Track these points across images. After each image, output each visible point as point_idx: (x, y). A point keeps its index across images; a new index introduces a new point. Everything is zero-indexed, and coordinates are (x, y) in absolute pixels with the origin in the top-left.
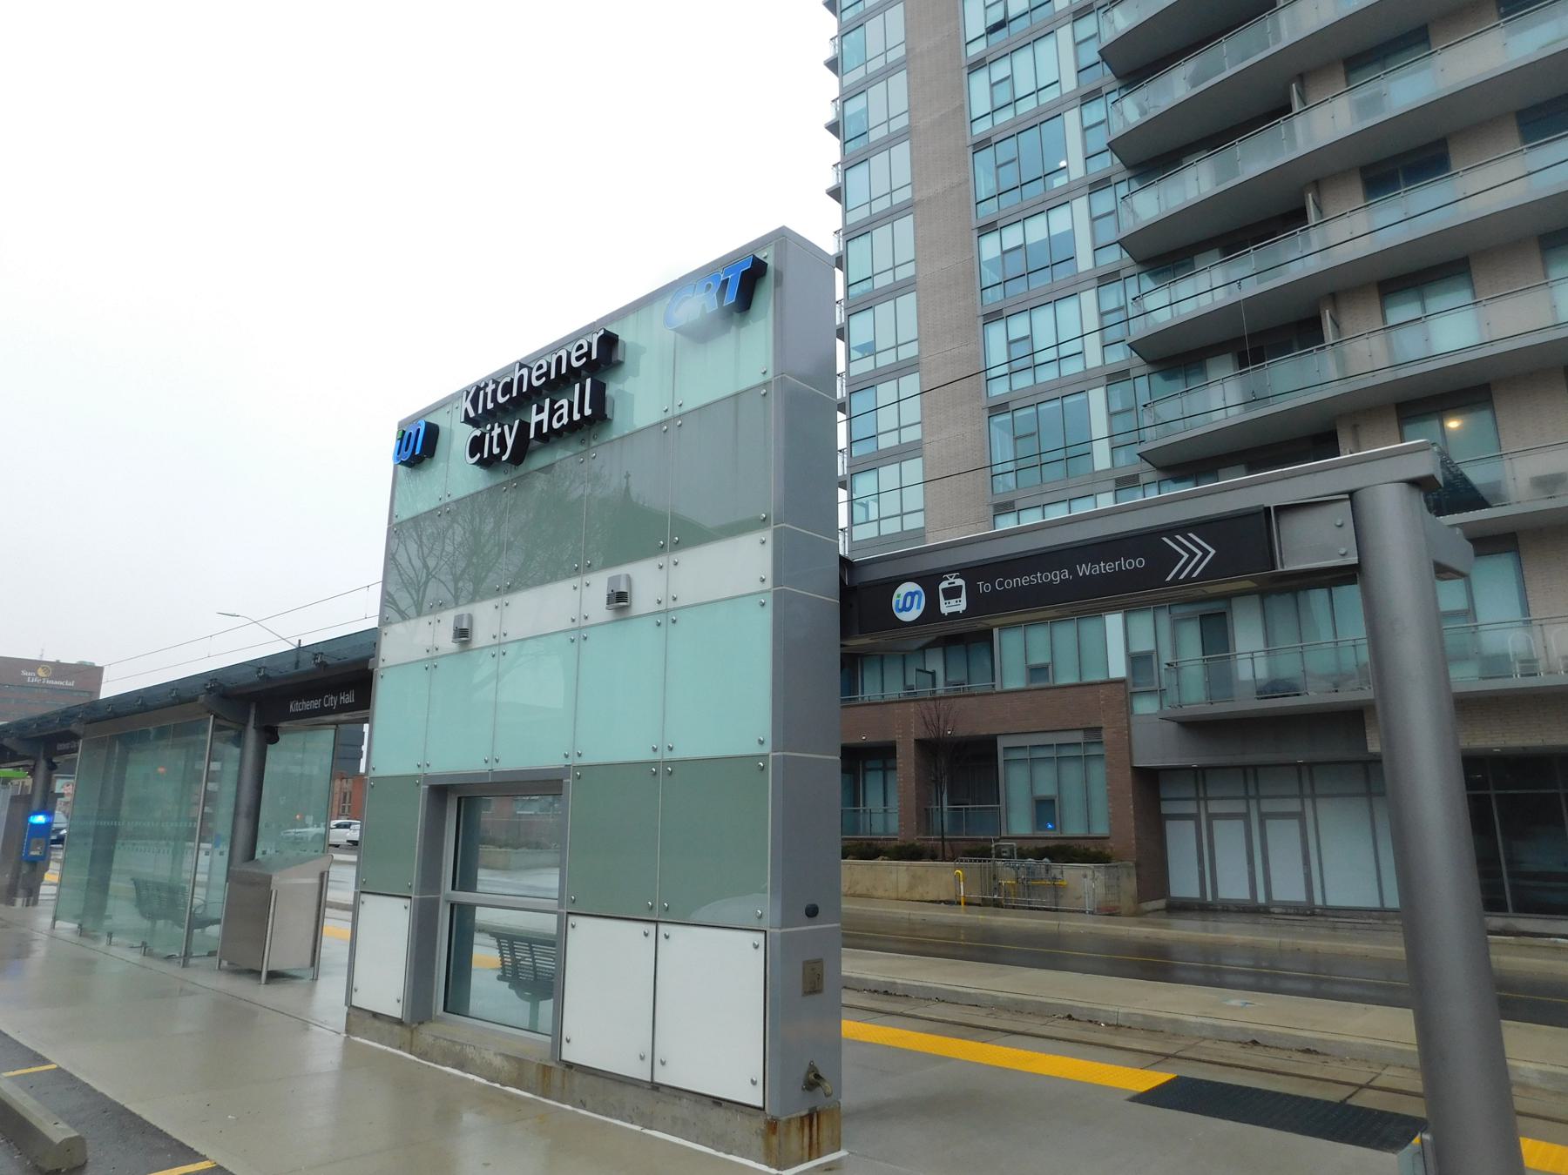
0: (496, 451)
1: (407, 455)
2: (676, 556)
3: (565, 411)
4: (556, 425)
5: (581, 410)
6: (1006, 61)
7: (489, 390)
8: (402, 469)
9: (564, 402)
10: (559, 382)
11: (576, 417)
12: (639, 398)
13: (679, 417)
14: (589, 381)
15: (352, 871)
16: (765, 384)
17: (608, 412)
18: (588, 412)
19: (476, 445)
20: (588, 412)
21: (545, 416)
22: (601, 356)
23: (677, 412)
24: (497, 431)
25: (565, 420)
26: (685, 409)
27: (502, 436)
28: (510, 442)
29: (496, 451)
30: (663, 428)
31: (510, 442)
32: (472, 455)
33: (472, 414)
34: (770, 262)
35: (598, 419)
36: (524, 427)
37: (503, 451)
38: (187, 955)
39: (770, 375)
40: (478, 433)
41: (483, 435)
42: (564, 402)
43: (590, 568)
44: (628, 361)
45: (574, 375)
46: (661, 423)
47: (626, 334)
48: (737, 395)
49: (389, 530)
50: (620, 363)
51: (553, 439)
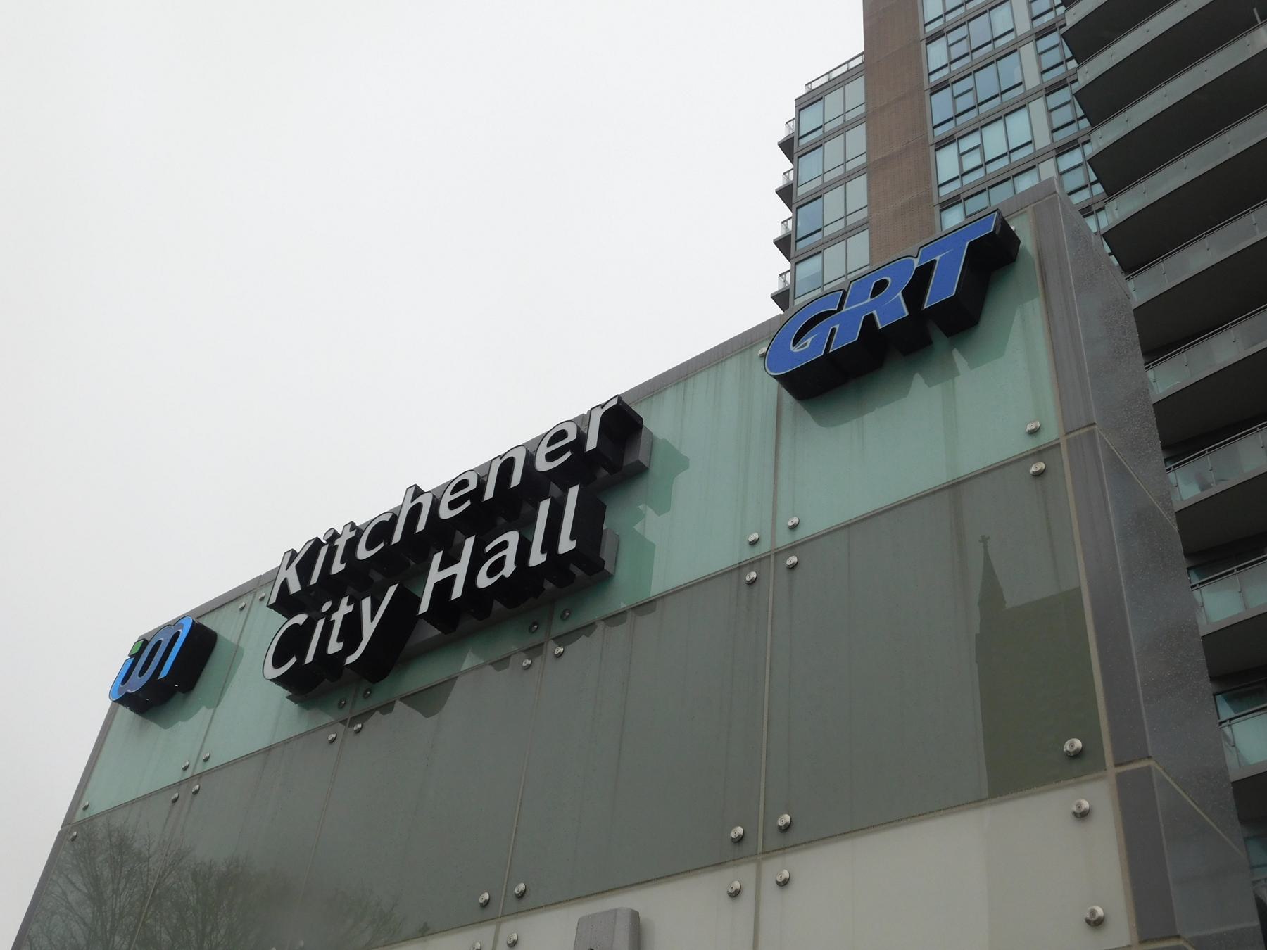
0: (334, 647)
1: (137, 682)
2: (779, 867)
3: (510, 553)
4: (483, 581)
5: (550, 542)
6: (977, 134)
7: (341, 544)
8: (125, 712)
9: (512, 537)
10: (494, 503)
11: (537, 558)
12: (677, 538)
13: (792, 549)
14: (573, 492)
15: (1036, 182)
16: (1038, 454)
17: (606, 554)
18: (566, 544)
19: (291, 644)
20: (566, 544)
21: (460, 570)
22: (609, 453)
23: (784, 539)
24: (345, 608)
25: (509, 569)
26: (801, 534)
27: (353, 621)
28: (369, 628)
29: (334, 647)
30: (743, 580)
31: (369, 628)
32: (278, 662)
33: (295, 587)
34: (1027, 241)
35: (577, 576)
36: (407, 600)
37: (349, 648)
38: (1252, 867)
39: (1052, 432)
40: (300, 619)
41: (310, 624)
42: (512, 537)
43: (523, 903)
44: (656, 469)
45: (536, 484)
46: (740, 568)
47: (658, 422)
48: (955, 486)
49: (61, 836)
50: (640, 470)
51: (467, 623)
